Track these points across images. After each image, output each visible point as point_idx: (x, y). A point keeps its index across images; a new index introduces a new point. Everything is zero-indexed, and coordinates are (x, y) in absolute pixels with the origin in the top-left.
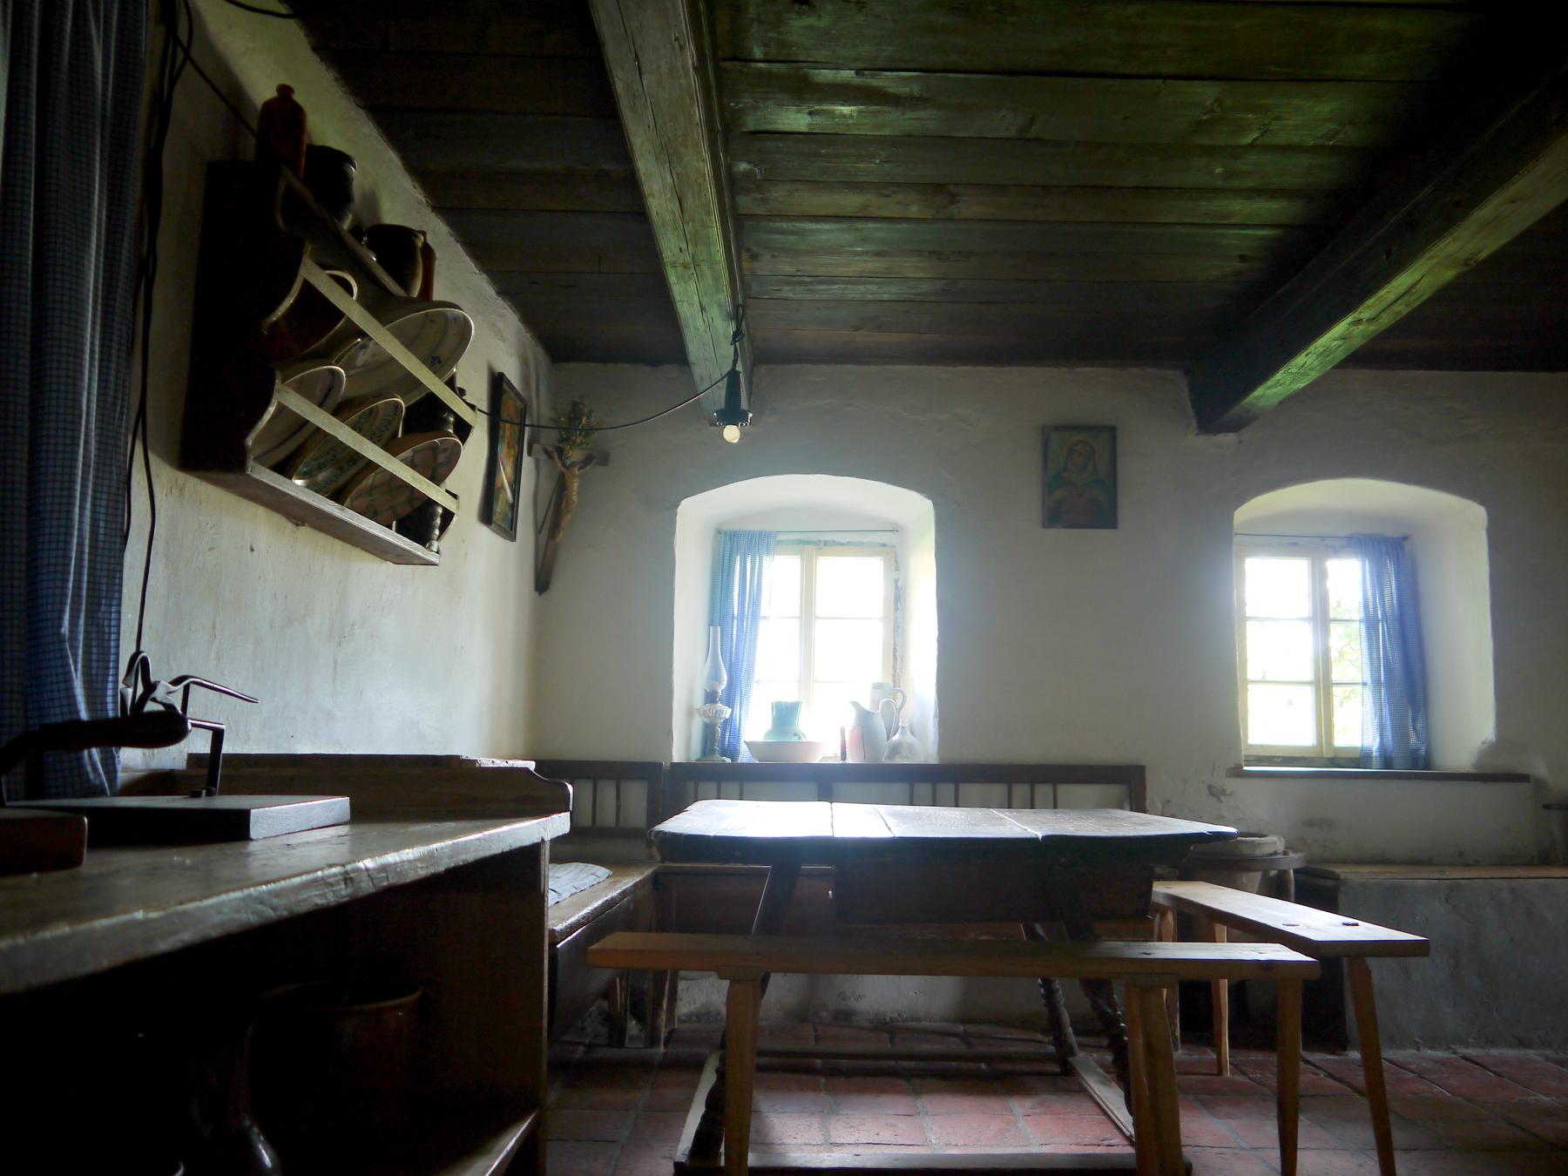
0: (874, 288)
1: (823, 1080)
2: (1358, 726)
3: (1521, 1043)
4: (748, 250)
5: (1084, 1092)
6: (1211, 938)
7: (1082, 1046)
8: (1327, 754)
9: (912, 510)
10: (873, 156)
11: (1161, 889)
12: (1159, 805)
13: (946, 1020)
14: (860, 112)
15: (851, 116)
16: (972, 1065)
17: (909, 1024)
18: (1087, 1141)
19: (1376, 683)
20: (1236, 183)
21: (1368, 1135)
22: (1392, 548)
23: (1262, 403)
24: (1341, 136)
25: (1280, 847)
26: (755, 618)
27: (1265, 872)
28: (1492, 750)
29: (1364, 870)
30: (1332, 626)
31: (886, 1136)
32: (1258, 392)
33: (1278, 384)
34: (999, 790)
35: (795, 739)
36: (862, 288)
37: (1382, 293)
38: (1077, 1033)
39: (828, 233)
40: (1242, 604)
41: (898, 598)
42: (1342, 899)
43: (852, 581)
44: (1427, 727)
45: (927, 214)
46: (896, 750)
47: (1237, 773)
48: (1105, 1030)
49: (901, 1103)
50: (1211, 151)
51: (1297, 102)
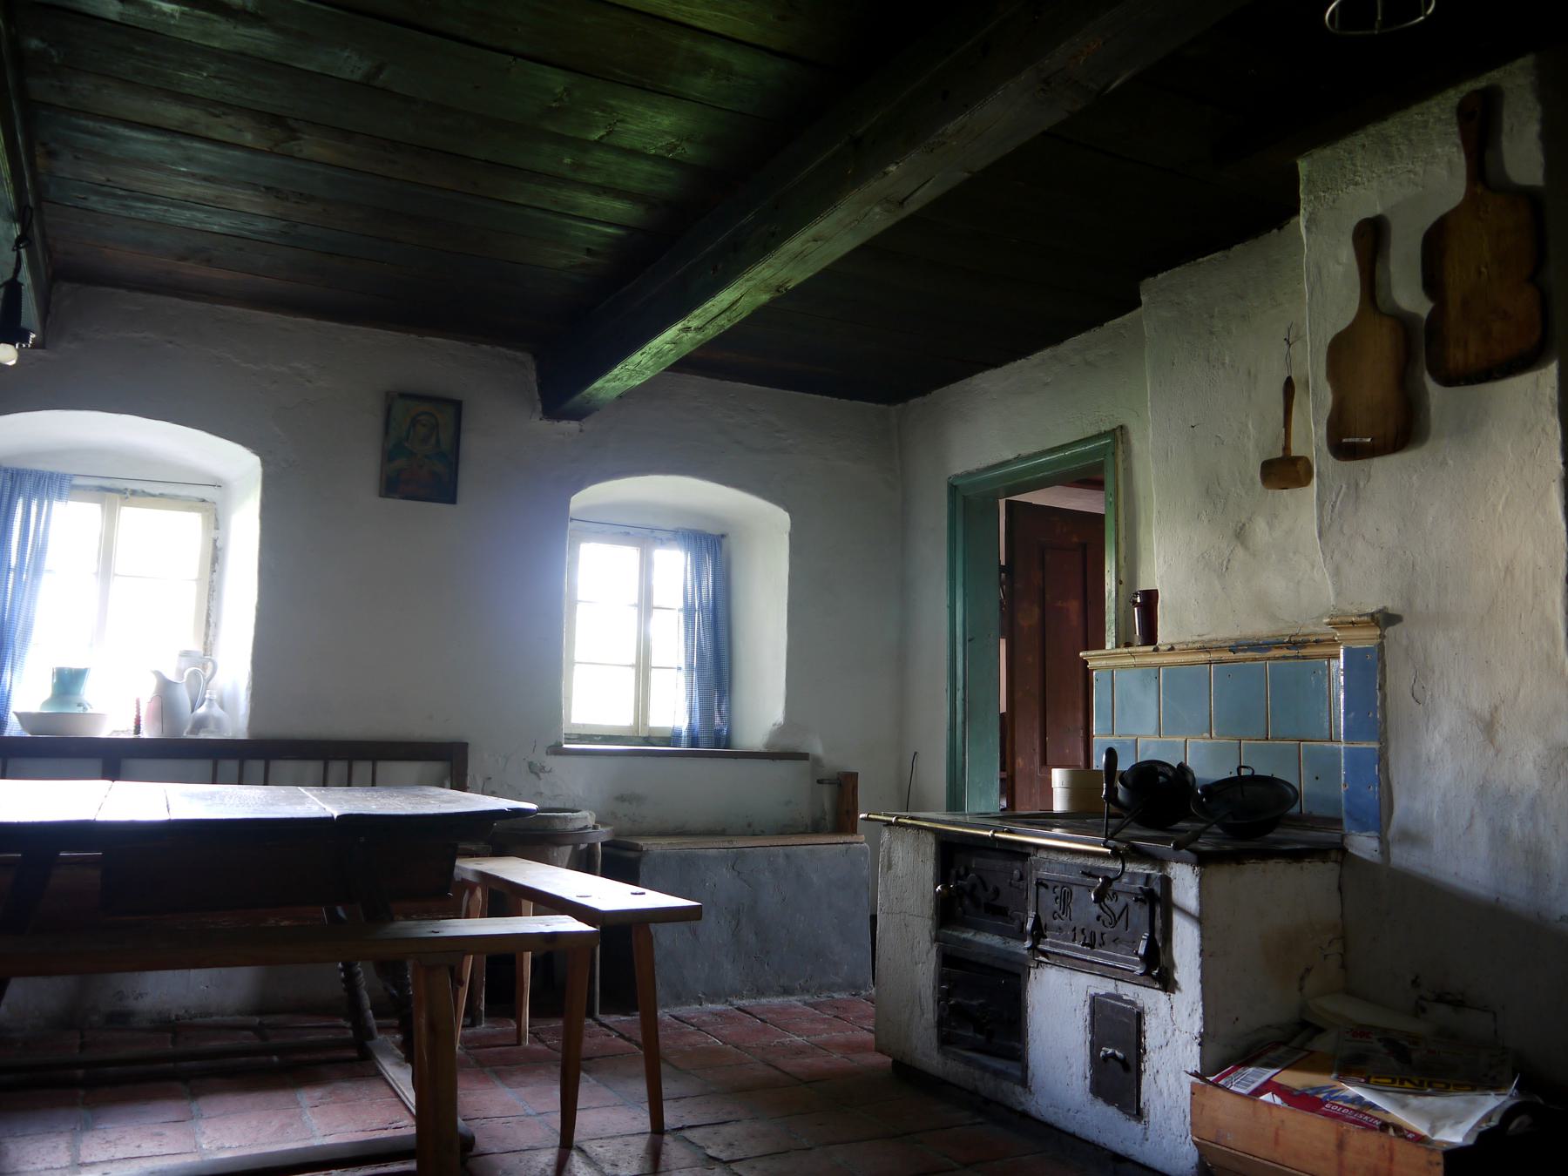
0: (201, 216)
1: (82, 1092)
2: (673, 709)
3: (787, 991)
4: (44, 145)
5: (379, 1076)
6: (516, 912)
7: (381, 1028)
8: (643, 734)
9: (237, 466)
10: (200, 68)
11: (469, 866)
12: (480, 783)
13: (240, 1013)
14: (183, 13)
15: (172, 16)
16: (263, 1059)
17: (199, 1020)
18: (375, 1126)
19: (690, 667)
20: (583, 177)
21: (641, 1088)
22: (712, 545)
23: (602, 395)
24: (679, 150)
25: (591, 822)
26: (37, 570)
27: (576, 846)
28: (781, 731)
29: (664, 841)
30: (656, 613)
31: (149, 1147)
32: (598, 384)
33: (616, 378)
34: (314, 767)
35: (79, 710)
36: (188, 214)
37: (708, 305)
38: (376, 1016)
39: (143, 143)
40: (573, 588)
41: (215, 557)
42: (643, 870)
43: (163, 539)
44: (729, 710)
45: (263, 145)
46: (200, 723)
47: (557, 750)
48: (399, 1012)
49: (172, 1109)
50: (561, 140)
51: (639, 109)
